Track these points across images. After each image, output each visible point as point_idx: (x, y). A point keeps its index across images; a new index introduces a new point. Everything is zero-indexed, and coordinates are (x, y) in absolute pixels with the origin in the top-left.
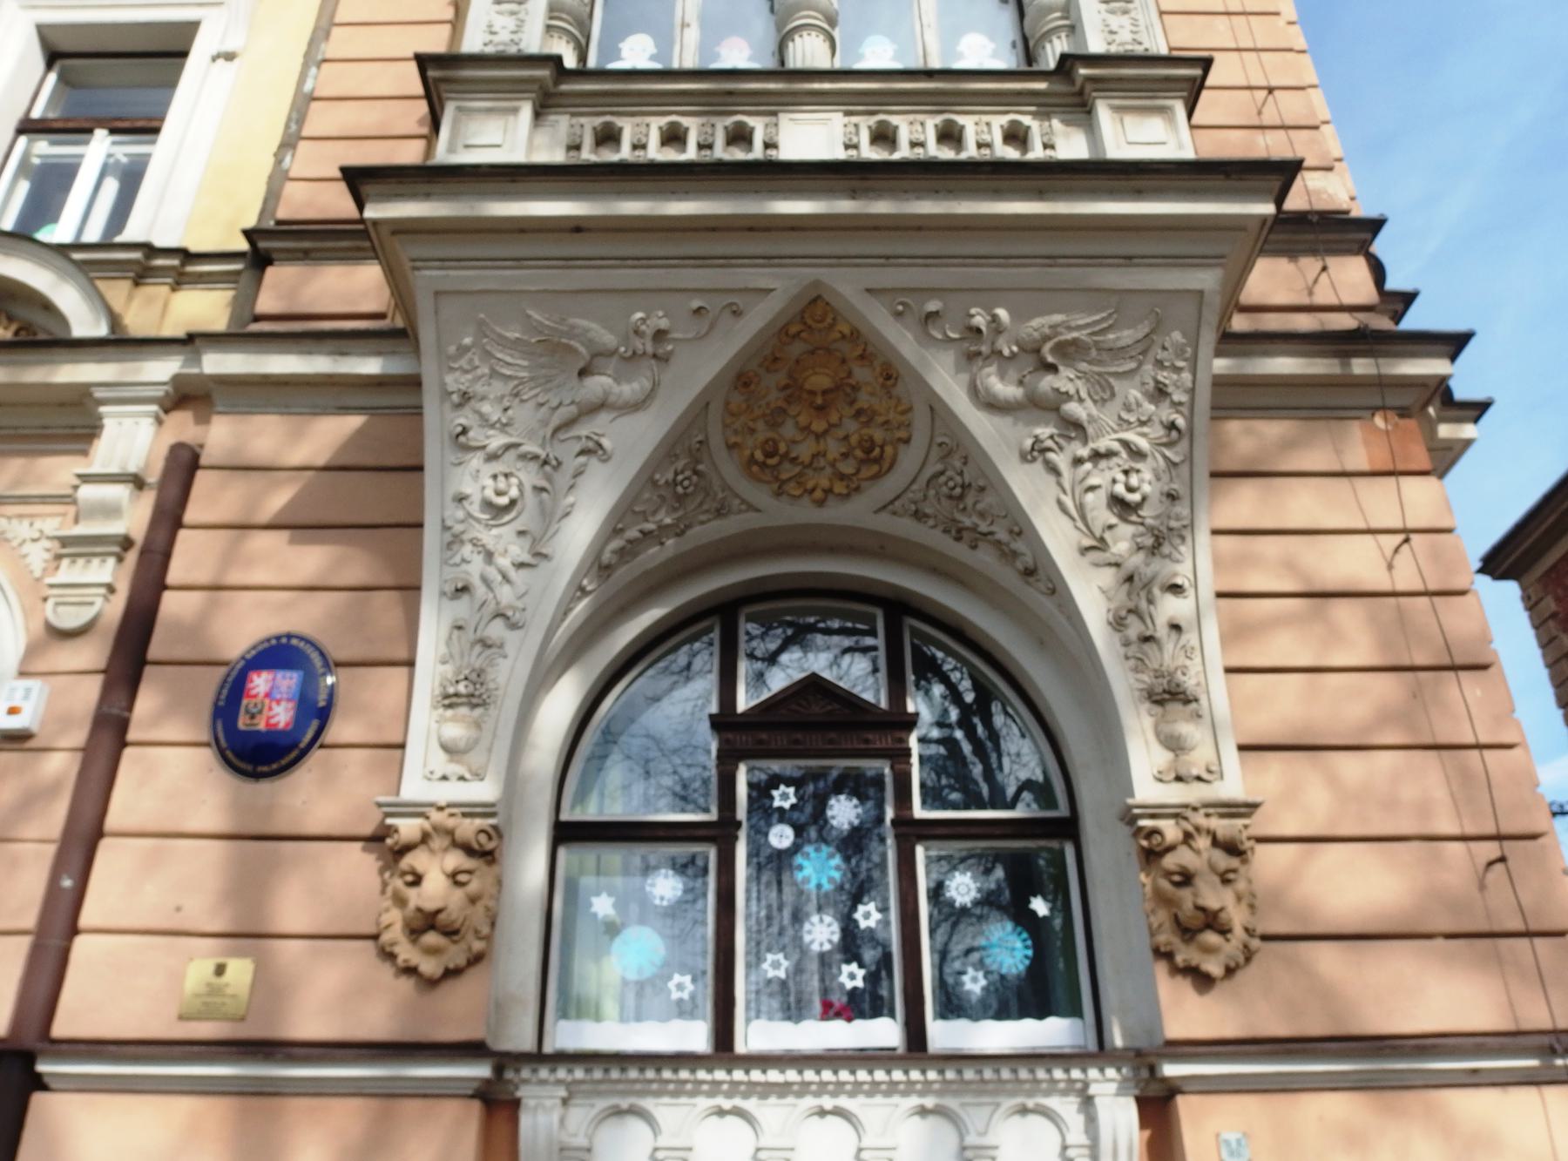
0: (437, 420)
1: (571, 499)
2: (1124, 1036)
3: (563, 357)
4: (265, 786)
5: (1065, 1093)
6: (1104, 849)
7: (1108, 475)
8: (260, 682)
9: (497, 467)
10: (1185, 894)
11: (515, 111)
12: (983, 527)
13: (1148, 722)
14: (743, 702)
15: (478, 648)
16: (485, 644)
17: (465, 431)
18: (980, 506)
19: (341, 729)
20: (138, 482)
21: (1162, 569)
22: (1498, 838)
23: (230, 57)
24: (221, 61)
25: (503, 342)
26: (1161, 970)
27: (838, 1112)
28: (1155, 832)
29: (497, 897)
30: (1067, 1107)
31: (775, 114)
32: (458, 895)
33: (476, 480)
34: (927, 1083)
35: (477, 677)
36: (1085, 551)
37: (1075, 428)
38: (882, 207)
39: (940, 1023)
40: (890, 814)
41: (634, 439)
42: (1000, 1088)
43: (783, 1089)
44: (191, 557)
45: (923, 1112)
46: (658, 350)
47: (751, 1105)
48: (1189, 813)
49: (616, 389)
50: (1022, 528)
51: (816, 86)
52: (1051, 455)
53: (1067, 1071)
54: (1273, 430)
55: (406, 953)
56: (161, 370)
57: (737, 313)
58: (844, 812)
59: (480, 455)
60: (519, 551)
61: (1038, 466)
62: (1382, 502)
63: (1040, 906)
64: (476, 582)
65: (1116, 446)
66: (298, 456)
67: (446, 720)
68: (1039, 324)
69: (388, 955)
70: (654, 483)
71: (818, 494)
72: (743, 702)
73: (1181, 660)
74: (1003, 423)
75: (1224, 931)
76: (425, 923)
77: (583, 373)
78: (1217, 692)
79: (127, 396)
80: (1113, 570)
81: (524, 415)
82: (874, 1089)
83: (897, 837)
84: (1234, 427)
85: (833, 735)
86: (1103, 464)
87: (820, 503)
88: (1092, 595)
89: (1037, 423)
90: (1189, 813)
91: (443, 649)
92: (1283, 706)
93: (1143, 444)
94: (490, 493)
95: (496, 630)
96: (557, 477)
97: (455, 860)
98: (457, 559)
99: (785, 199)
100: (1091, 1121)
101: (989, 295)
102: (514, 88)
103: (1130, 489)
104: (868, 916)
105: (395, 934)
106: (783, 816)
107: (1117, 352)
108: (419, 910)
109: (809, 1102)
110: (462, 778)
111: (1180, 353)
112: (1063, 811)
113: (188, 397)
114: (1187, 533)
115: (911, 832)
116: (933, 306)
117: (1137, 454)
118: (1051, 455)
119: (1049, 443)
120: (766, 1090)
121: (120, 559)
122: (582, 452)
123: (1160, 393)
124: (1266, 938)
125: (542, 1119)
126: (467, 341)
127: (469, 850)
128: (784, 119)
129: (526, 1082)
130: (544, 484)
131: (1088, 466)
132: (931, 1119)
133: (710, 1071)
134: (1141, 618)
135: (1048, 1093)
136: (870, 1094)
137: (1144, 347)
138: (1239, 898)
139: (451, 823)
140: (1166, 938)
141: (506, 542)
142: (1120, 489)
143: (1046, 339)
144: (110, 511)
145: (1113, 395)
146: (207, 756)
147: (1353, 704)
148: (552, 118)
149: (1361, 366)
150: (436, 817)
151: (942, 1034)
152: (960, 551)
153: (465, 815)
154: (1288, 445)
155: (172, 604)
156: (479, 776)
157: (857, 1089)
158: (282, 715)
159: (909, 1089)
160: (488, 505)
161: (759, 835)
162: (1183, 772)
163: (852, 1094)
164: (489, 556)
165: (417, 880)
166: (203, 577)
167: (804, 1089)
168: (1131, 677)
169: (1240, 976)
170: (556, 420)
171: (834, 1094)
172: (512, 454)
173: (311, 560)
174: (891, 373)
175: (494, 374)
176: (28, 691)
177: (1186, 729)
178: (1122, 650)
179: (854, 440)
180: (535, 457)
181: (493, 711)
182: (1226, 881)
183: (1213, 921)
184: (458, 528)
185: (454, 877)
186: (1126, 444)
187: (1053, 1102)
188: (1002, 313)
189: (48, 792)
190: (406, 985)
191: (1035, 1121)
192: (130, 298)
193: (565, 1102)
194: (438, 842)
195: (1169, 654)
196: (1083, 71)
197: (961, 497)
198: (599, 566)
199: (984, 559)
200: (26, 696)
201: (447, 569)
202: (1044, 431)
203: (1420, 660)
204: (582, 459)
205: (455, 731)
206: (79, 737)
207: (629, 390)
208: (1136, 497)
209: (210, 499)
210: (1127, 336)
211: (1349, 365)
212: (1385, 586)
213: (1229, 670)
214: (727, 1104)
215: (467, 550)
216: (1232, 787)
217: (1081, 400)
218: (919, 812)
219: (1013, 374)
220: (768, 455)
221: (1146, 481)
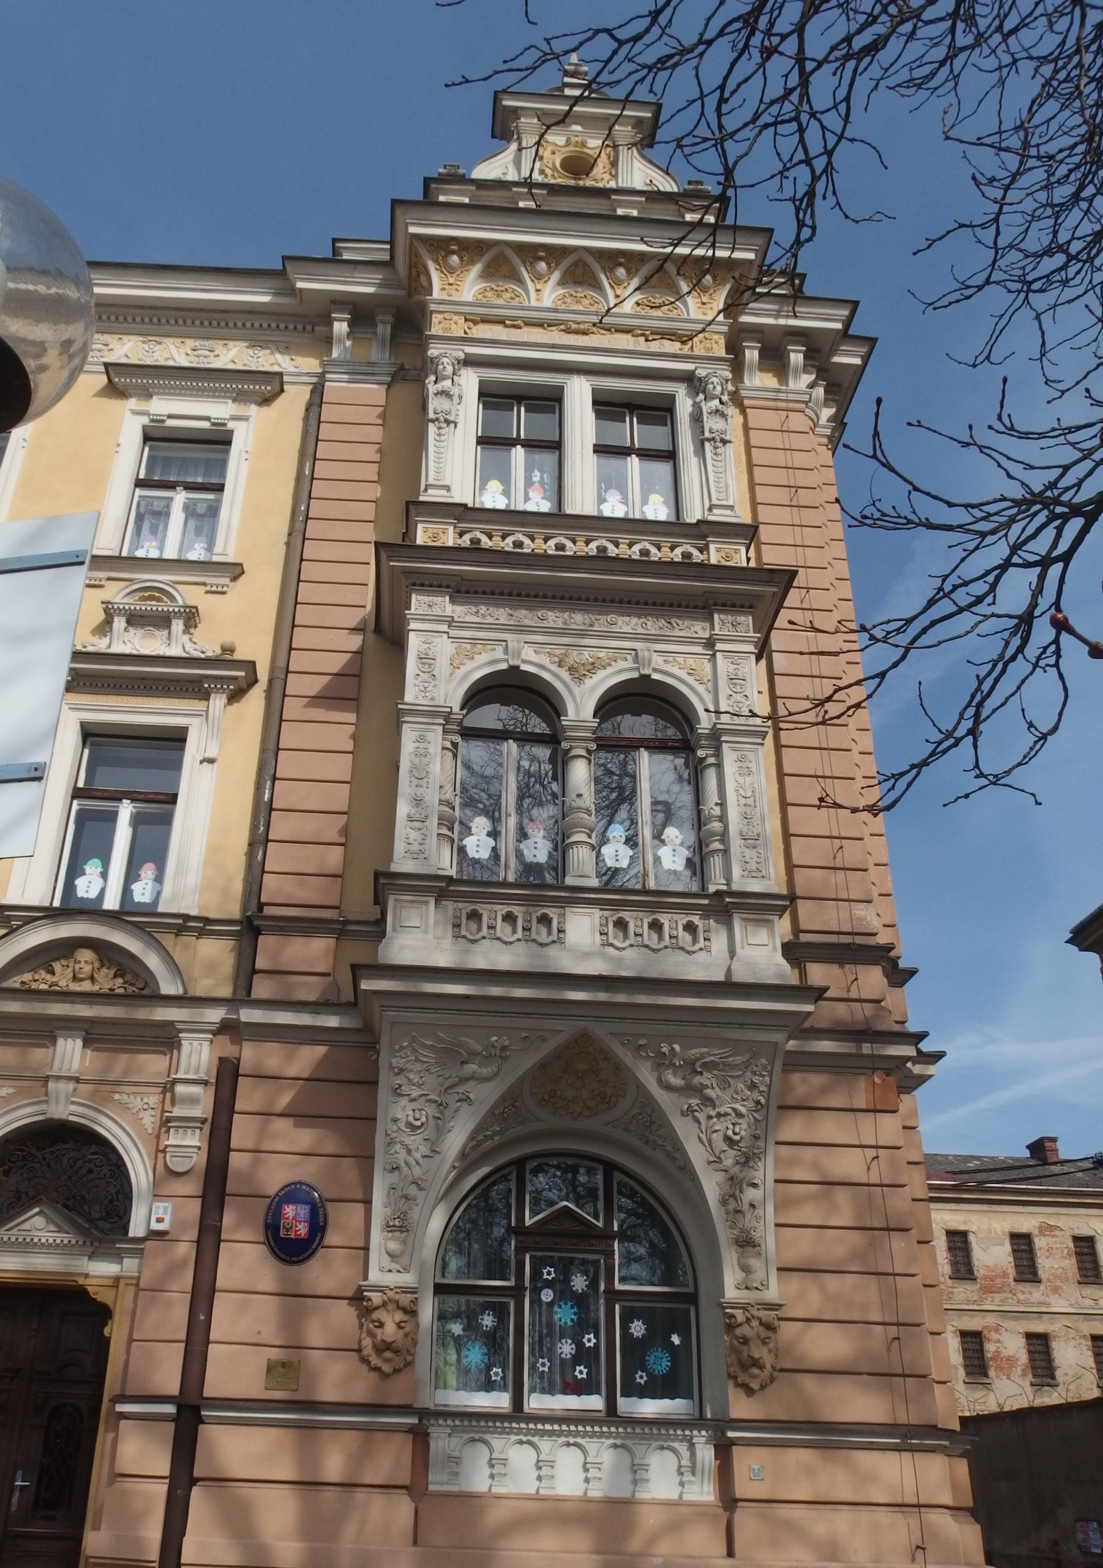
0: (385, 1080)
1: (452, 1124)
2: (712, 1414)
3: (452, 1054)
4: (295, 1268)
5: (681, 1441)
6: (709, 1318)
7: (725, 1125)
8: (289, 1210)
9: (414, 1105)
10: (745, 1349)
11: (426, 903)
12: (660, 1142)
13: (735, 1256)
14: (528, 1222)
15: (403, 1200)
16: (407, 1197)
17: (400, 1086)
18: (659, 1132)
19: (332, 1238)
20: (206, 1083)
21: (749, 1174)
22: (898, 1324)
23: (211, 761)
24: (205, 764)
25: (425, 1046)
26: (731, 1384)
27: (576, 1445)
28: (732, 1316)
29: (416, 1333)
30: (682, 1448)
31: (563, 907)
32: (401, 1333)
34: (618, 1433)
35: (403, 1216)
36: (710, 1163)
37: (709, 1102)
38: (621, 998)
39: (623, 1399)
40: (602, 1287)
41: (486, 1095)
42: (651, 1437)
43: (551, 1433)
44: (242, 1131)
45: (615, 1446)
46: (502, 1055)
47: (535, 1439)
48: (750, 1308)
49: (479, 1071)
50: (679, 1147)
51: (586, 896)
52: (696, 1114)
53: (683, 1431)
54: (817, 1080)
55: (375, 1361)
56: (215, 1015)
57: (544, 1040)
58: (579, 1283)
59: (407, 1098)
60: (424, 1149)
61: (690, 1118)
62: (870, 1129)
63: (676, 1339)
64: (403, 1164)
65: (730, 1111)
66: (293, 1071)
67: (390, 1239)
68: (695, 1052)
69: (365, 1361)
70: (493, 1113)
71: (575, 1115)
72: (528, 1222)
73: (754, 1223)
74: (674, 1096)
75: (761, 1368)
76: (382, 1347)
77: (462, 1063)
78: (770, 1240)
79: (195, 1028)
80: (723, 1173)
81: (430, 1080)
82: (593, 1435)
83: (606, 1299)
84: (796, 1077)
85: (575, 1241)
86: (722, 1119)
87: (576, 1119)
88: (711, 1186)
89: (690, 1097)
90: (750, 1308)
91: (386, 1200)
92: (803, 1246)
93: (743, 1110)
94: (411, 1119)
95: (412, 1190)
96: (446, 1112)
97: (399, 1316)
98: (392, 1151)
99: (573, 990)
100: (693, 1455)
101: (670, 1039)
102: (426, 890)
103: (735, 1134)
104: (589, 1340)
105: (368, 1350)
106: (549, 1284)
107: (733, 1067)
108: (383, 1341)
109: (563, 1439)
110: (399, 1271)
111: (765, 1068)
112: (690, 1290)
113: (226, 1028)
114: (762, 1156)
115: (613, 1295)
116: (642, 1042)
117: (740, 1115)
118: (696, 1114)
119: (696, 1108)
120: (543, 1433)
121: (201, 1129)
122: (458, 1101)
123: (753, 1086)
124: (782, 1370)
125: (440, 1443)
126: (405, 1044)
127: (405, 1310)
128: (569, 911)
129: (432, 1425)
130: (438, 1115)
131: (715, 1120)
132: (619, 1450)
133: (518, 1423)
134: (736, 1199)
135: (673, 1441)
136: (591, 1437)
137: (747, 1065)
138: (770, 1351)
139: (397, 1297)
141: (415, 1141)
142: (730, 1133)
143: (698, 1059)
144: (193, 1100)
145: (730, 1086)
146: (263, 1249)
147: (839, 1246)
148: (444, 903)
149: (866, 1049)
150: (390, 1294)
151: (626, 1405)
153: (403, 1292)
154: (824, 1090)
155: (237, 1160)
156: (407, 1270)
157: (585, 1435)
158: (303, 1230)
159: (609, 1435)
160: (409, 1125)
161: (536, 1292)
162: (749, 1285)
163: (583, 1437)
164: (409, 1152)
165: (381, 1325)
166: (250, 1145)
167: (561, 1434)
168: (729, 1231)
169: (767, 1389)
170: (447, 1084)
171: (574, 1437)
172: (423, 1099)
173: (305, 1137)
174: (618, 1067)
175: (417, 1060)
176: (165, 1208)
177: (753, 1262)
178: (725, 1216)
179: (596, 1092)
180: (436, 1101)
181: (412, 1235)
182: (764, 1343)
183: (757, 1363)
184: (394, 1135)
185: (399, 1325)
186: (734, 1110)
187: (676, 1445)
188: (677, 1047)
189: (180, 1265)
190: (374, 1375)
191: (667, 1453)
192: (175, 945)
193: (449, 1435)
194: (391, 1307)
195: (748, 1220)
196: (727, 900)
197: (649, 1127)
198: (463, 1155)
200: (165, 1213)
201: (387, 1157)
202: (694, 1102)
203: (875, 1225)
204: (459, 1104)
205: (393, 1246)
206: (194, 1234)
207: (485, 1071)
208: (737, 1138)
209: (248, 1097)
210: (738, 1059)
211: (861, 1047)
212: (865, 1181)
213: (777, 1225)
214: (524, 1439)
215: (398, 1147)
216: (772, 1294)
217: (713, 1088)
218: (618, 1286)
219: (680, 1074)
220: (551, 1097)
221: (743, 1129)
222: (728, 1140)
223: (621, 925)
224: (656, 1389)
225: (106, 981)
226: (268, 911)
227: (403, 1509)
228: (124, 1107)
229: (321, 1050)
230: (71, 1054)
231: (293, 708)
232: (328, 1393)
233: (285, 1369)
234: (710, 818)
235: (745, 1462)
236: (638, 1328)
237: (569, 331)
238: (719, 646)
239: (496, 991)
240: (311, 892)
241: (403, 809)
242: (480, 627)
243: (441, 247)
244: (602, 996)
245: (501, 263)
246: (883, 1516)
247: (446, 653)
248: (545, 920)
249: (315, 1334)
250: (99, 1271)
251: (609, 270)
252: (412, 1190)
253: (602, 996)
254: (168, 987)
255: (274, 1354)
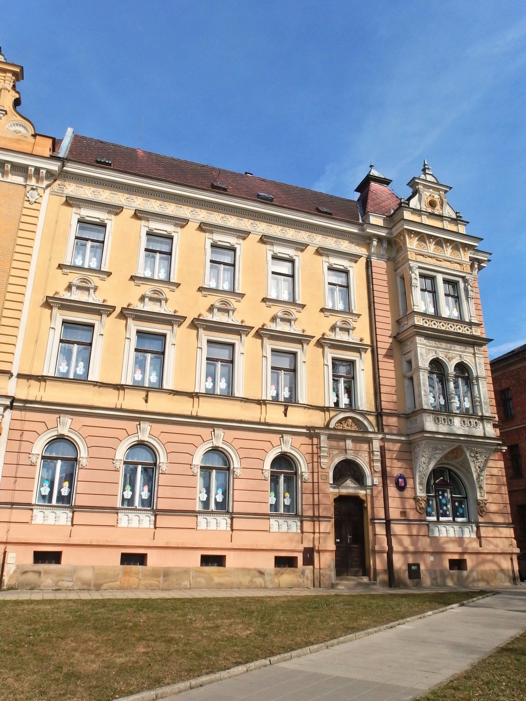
6: (471, 501)
8: (400, 480)
19: (408, 486)
33: (423, 460)
37: (478, 459)
38: (469, 439)
44: (388, 463)
50: (470, 467)
66: (395, 449)
69: (417, 511)
88: (475, 476)
95: (423, 476)
113: (382, 439)
123: (486, 457)
140: (480, 512)
141: (424, 466)
151: (441, 519)
152: (461, 468)
155: (388, 469)
158: (403, 484)
195: (481, 483)
199: (464, 469)
205: (421, 488)
206: (381, 485)
207: (440, 452)
213: (211, 261)
216: (485, 498)
222: (479, 467)
223: (464, 422)
224: (462, 516)
225: (354, 428)
226: (384, 411)
227: (428, 540)
228: (361, 456)
229: (400, 444)
230: (349, 444)
231: (381, 358)
232: (411, 518)
233: (404, 513)
234: (476, 397)
235: (483, 530)
236: (457, 504)
237: (437, 260)
238: (476, 355)
239: (448, 437)
240: (391, 406)
241: (423, 393)
242: (430, 346)
243: (410, 232)
244: (466, 439)
245: (423, 238)
246: (504, 539)
247: (425, 352)
248: (450, 420)
249: (407, 506)
250: (362, 493)
251: (446, 243)
252: (423, 476)
253: (466, 439)
254: (370, 430)
255: (401, 510)
